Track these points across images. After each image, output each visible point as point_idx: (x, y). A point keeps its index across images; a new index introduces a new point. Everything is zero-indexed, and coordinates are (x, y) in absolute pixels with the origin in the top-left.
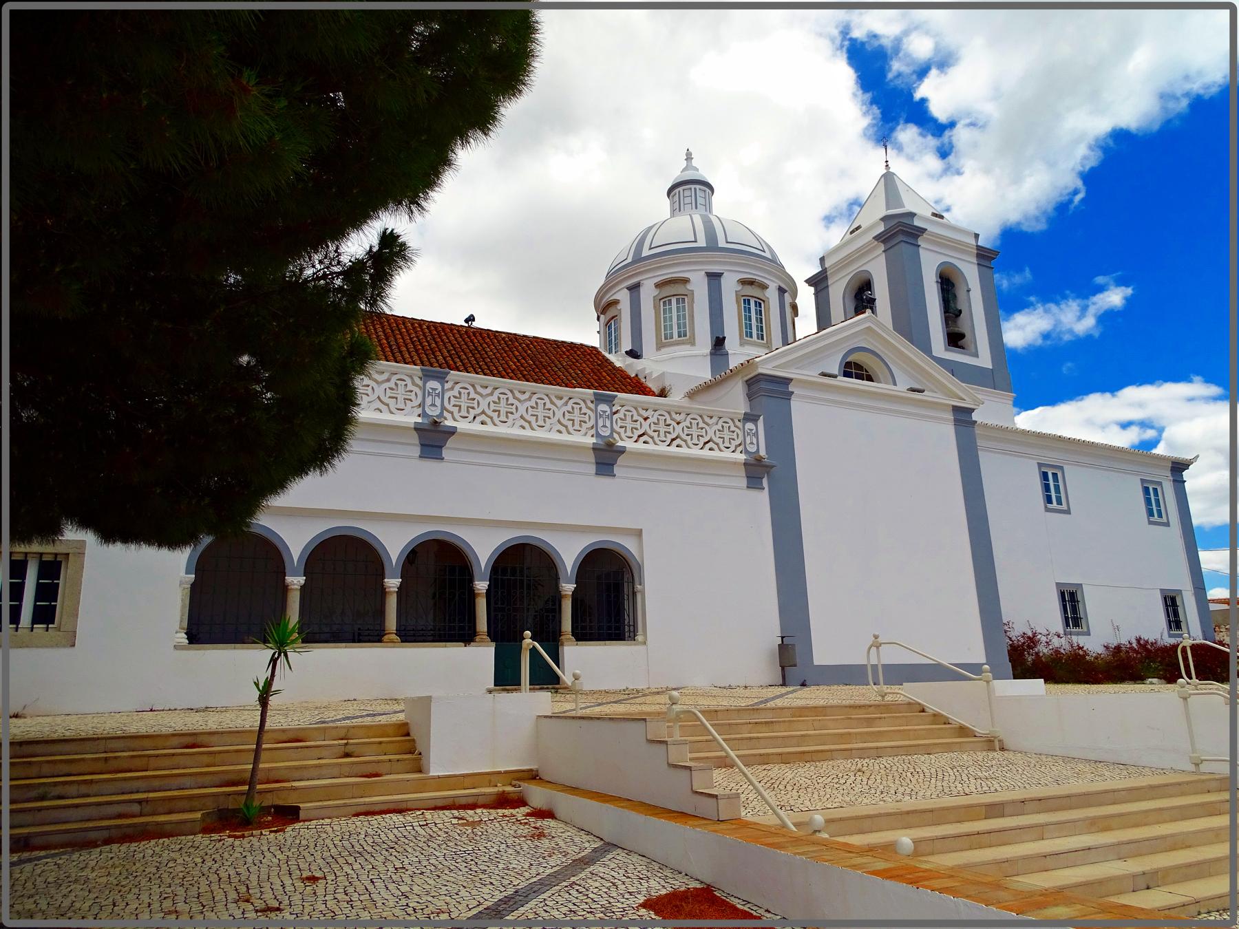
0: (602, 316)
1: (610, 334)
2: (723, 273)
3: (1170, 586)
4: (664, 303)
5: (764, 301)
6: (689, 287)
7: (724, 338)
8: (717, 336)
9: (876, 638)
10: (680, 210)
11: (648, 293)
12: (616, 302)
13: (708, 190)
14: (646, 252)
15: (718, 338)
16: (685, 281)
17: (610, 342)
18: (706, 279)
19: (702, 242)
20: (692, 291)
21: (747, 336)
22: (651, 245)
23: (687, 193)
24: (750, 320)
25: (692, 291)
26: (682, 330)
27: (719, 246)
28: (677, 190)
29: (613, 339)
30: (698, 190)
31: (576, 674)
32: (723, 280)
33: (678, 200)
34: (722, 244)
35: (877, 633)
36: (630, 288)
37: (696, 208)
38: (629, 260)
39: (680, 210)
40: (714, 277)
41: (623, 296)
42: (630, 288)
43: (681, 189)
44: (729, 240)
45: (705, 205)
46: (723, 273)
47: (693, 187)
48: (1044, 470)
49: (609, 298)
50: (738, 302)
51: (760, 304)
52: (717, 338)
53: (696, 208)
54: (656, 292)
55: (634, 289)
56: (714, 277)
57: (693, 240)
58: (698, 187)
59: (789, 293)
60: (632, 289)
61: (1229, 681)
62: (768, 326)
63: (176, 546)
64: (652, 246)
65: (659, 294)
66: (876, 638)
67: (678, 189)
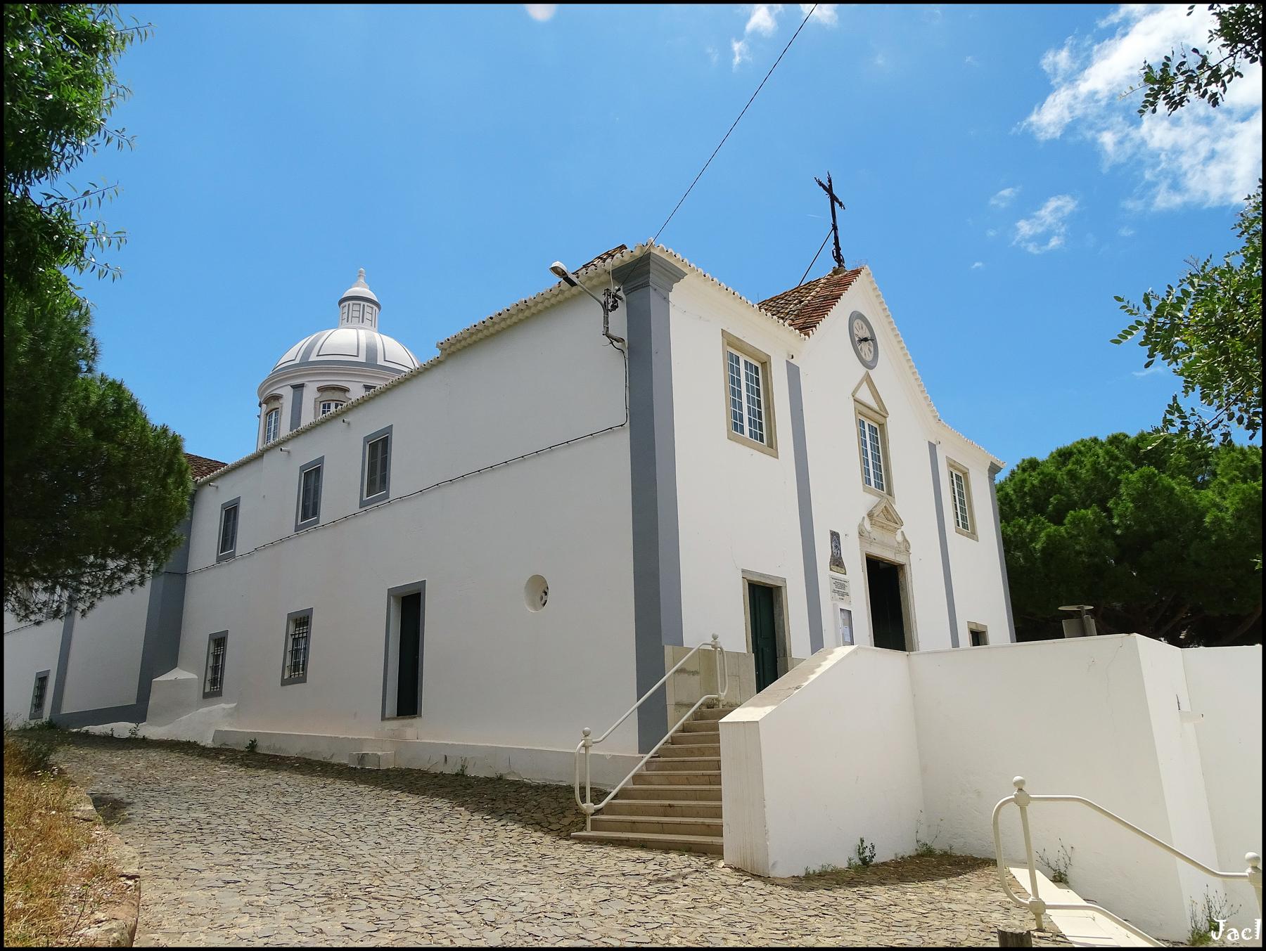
0: (264, 406)
1: (270, 423)
3: (768, 569)
4: (324, 407)
6: (348, 395)
11: (310, 395)
12: (277, 398)
13: (375, 308)
14: (313, 358)
16: (345, 390)
17: (269, 430)
19: (362, 359)
22: (319, 352)
23: (356, 308)
28: (347, 303)
29: (273, 421)
33: (346, 317)
34: (380, 362)
35: (717, 633)
36: (294, 387)
37: (363, 322)
38: (297, 361)
41: (287, 393)
42: (294, 387)
43: (351, 302)
47: (362, 303)
48: (863, 418)
49: (272, 391)
53: (363, 322)
55: (298, 388)
58: (366, 304)
60: (296, 388)
61: (974, 645)
63: (1019, 489)
64: (320, 354)
65: (320, 396)
67: (348, 302)
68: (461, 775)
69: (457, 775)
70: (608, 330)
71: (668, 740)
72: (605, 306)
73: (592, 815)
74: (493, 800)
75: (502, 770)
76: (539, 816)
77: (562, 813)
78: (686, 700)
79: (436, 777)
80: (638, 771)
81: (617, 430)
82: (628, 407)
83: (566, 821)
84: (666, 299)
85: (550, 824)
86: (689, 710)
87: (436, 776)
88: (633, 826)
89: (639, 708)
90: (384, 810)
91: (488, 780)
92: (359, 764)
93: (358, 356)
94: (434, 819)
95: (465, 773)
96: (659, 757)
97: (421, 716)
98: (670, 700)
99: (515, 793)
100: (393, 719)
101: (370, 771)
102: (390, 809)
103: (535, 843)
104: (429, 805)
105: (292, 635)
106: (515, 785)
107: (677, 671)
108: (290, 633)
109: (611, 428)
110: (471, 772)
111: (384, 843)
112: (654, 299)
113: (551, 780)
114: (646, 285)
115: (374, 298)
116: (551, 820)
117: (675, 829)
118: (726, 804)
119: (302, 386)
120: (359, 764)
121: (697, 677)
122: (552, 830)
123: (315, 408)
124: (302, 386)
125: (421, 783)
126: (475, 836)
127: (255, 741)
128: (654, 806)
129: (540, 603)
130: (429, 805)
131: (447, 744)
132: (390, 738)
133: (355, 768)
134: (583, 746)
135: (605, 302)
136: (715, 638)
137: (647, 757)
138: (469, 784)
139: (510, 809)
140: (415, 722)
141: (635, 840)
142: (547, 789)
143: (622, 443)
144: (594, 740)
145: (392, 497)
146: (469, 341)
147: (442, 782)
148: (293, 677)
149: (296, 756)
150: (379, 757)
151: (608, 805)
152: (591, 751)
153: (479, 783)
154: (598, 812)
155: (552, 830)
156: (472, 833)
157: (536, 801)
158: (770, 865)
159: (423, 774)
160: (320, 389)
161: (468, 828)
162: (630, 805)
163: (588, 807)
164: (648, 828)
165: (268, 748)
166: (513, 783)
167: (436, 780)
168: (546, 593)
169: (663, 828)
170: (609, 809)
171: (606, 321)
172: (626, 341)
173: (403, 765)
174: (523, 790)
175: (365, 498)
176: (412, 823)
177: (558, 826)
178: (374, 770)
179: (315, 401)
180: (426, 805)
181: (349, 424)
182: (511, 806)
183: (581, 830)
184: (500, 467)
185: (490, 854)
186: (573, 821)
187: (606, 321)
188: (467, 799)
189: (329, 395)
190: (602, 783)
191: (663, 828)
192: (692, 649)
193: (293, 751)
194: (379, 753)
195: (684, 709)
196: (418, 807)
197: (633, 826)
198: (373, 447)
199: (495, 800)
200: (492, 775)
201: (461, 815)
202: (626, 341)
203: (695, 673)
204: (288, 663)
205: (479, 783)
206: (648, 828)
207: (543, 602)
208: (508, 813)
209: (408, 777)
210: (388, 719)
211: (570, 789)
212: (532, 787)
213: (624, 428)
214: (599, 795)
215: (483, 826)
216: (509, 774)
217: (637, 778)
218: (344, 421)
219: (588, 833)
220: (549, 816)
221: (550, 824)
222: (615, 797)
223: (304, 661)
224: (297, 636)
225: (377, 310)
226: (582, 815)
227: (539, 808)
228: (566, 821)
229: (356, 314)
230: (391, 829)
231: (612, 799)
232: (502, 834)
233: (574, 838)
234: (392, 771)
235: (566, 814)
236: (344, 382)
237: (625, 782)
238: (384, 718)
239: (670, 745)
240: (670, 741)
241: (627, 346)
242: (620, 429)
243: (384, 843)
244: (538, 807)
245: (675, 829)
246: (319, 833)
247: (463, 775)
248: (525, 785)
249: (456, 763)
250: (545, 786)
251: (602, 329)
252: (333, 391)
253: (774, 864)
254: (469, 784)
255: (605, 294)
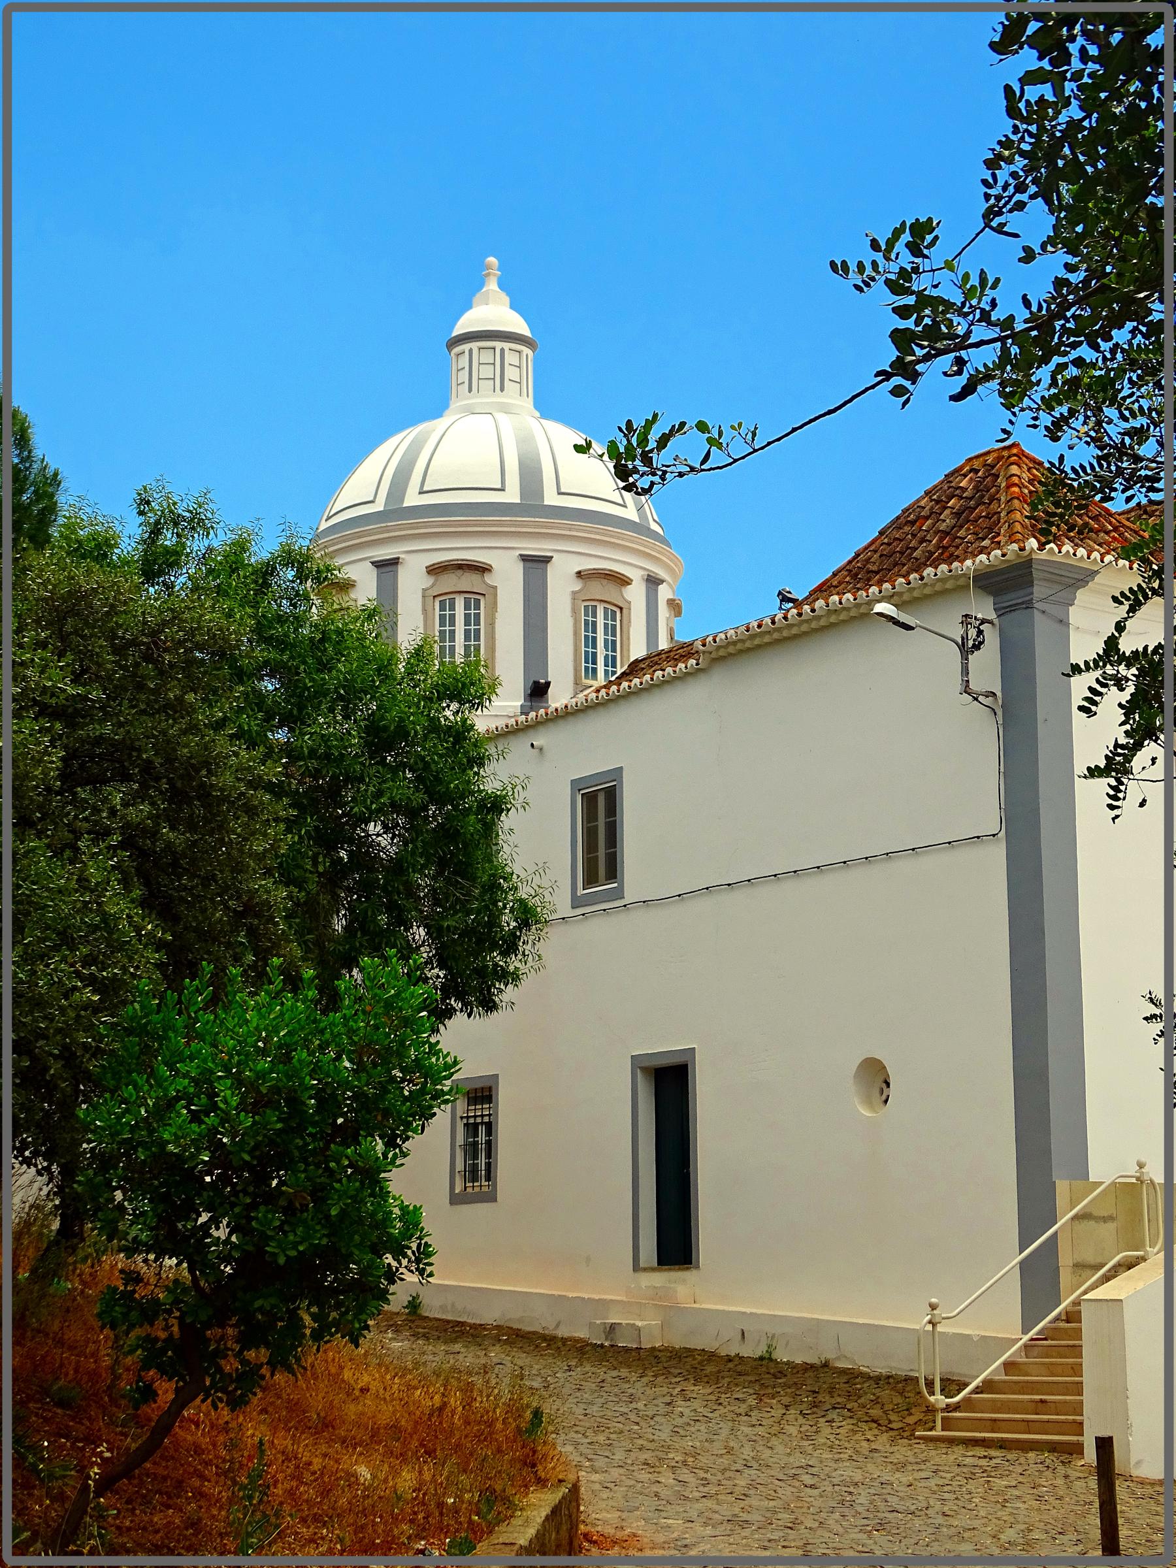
2: (552, 557)
5: (621, 609)
6: (489, 579)
7: (548, 684)
8: (536, 679)
9: (1141, 1168)
10: (470, 390)
13: (526, 351)
14: (412, 499)
15: (536, 684)
16: (482, 569)
18: (521, 565)
19: (512, 496)
20: (495, 588)
21: (587, 677)
23: (487, 357)
24: (594, 646)
25: (495, 588)
26: (472, 612)
27: (546, 503)
28: (466, 347)
30: (507, 352)
31: (869, 1103)
32: (550, 568)
34: (551, 499)
35: (1143, 1160)
36: (379, 565)
37: (502, 389)
38: (379, 506)
39: (470, 390)
40: (536, 564)
42: (379, 565)
43: (474, 345)
44: (563, 490)
45: (519, 367)
46: (552, 557)
47: (498, 345)
50: (575, 611)
51: (614, 613)
52: (536, 683)
53: (502, 389)
54: (428, 581)
55: (387, 566)
56: (536, 564)
57: (499, 486)
58: (507, 346)
59: (669, 584)
62: (625, 647)
64: (425, 489)
65: (432, 586)
66: (1141, 1168)
68: (766, 1360)
69: (761, 1358)
70: (967, 686)
71: (1060, 1314)
72: (962, 646)
73: (943, 1410)
74: (814, 1392)
75: (830, 1355)
76: (876, 1412)
77: (907, 1410)
78: (1090, 1258)
79: (730, 1361)
80: (1009, 1357)
81: (986, 840)
82: (1003, 806)
83: (911, 1420)
84: (1064, 623)
85: (890, 1422)
86: (1093, 1275)
87: (729, 1359)
88: (994, 1425)
89: (1022, 1264)
90: (668, 1399)
91: (808, 1367)
92: (606, 1339)
93: (502, 490)
94: (738, 1411)
95: (774, 1356)
96: (1045, 1339)
97: (698, 1267)
98: (1065, 1260)
99: (847, 1385)
100: (653, 1269)
101: (627, 1350)
102: (675, 1399)
103: (868, 1440)
104: (727, 1396)
105: (462, 1118)
106: (847, 1374)
107: (1076, 1218)
108: (459, 1113)
109: (978, 837)
110: (782, 1356)
111: (682, 1432)
112: (1041, 625)
113: (899, 1369)
114: (1028, 605)
115: (523, 329)
116: (892, 1418)
117: (1044, 1427)
118: (1088, 1398)
119: (394, 562)
120: (606, 1339)
121: (1111, 1226)
122: (892, 1429)
123: (424, 610)
124: (394, 562)
125: (709, 1369)
126: (793, 1430)
127: (418, 1296)
128: (1022, 1401)
129: (877, 1099)
130: (727, 1396)
131: (744, 1313)
132: (653, 1300)
133: (602, 1346)
134: (930, 1322)
135: (963, 638)
136: (1141, 1166)
137: (1026, 1338)
138: (779, 1372)
139: (838, 1403)
140: (689, 1276)
141: (992, 1440)
142: (891, 1380)
143: (998, 854)
144: (943, 1315)
145: (630, 896)
146: (748, 644)
147: (739, 1368)
148: (469, 1190)
149: (495, 1324)
150: (639, 1329)
151: (966, 1400)
152: (939, 1328)
153: (795, 1371)
154: (949, 1408)
155: (892, 1429)
156: (787, 1427)
157: (874, 1394)
158: (1133, 1462)
159: (711, 1356)
160: (435, 570)
161: (782, 1422)
162: (993, 1400)
163: (938, 1399)
164: (1011, 1425)
165: (443, 1308)
166: (844, 1371)
167: (730, 1365)
168: (888, 1085)
169: (1028, 1426)
170: (967, 1404)
171: (965, 671)
172: (999, 694)
173: (678, 1341)
174: (857, 1380)
175: (581, 892)
176: (710, 1415)
177: (900, 1425)
178: (631, 1349)
179: (424, 597)
180: (723, 1396)
181: (541, 749)
182: (839, 1400)
183: (931, 1430)
184: (808, 874)
185: (811, 1447)
186: (920, 1420)
187: (965, 671)
188: (778, 1390)
189: (451, 582)
190: (959, 1370)
191: (1028, 1426)
192: (1102, 1183)
193: (489, 1315)
194: (639, 1324)
195: (1089, 1272)
196: (712, 1397)
197: (994, 1425)
198: (590, 800)
199: (818, 1392)
200: (812, 1359)
201: (772, 1408)
202: (999, 694)
203: (1105, 1219)
204: (460, 1166)
205: (795, 1371)
206: (1011, 1425)
207: (884, 1097)
208: (835, 1408)
209: (687, 1360)
210: (645, 1270)
211: (911, 1380)
212: (870, 1378)
213: (998, 838)
214: (951, 1385)
215: (801, 1420)
216: (838, 1358)
217: (1009, 1366)
218: (532, 745)
219: (938, 1432)
220: (891, 1412)
221: (890, 1422)
222: (977, 1390)
223: (488, 1165)
224: (472, 1121)
225: (530, 353)
226: (931, 1410)
227: (878, 1403)
228: (911, 1420)
229: (487, 372)
230: (685, 1419)
231: (971, 1393)
232: (826, 1430)
233: (919, 1438)
234: (660, 1351)
235: (913, 1411)
236: (477, 551)
237: (992, 1370)
238: (636, 1268)
239: (1063, 1325)
240: (1064, 1317)
241: (1000, 704)
242: (990, 840)
243: (682, 1432)
244: (876, 1402)
245: (1044, 1427)
246: (600, 1420)
247: (770, 1359)
248: (861, 1374)
249: (759, 1341)
250: (889, 1377)
251: (958, 686)
252: (460, 572)
253: (1137, 1463)
254: (779, 1372)
255: (962, 623)
